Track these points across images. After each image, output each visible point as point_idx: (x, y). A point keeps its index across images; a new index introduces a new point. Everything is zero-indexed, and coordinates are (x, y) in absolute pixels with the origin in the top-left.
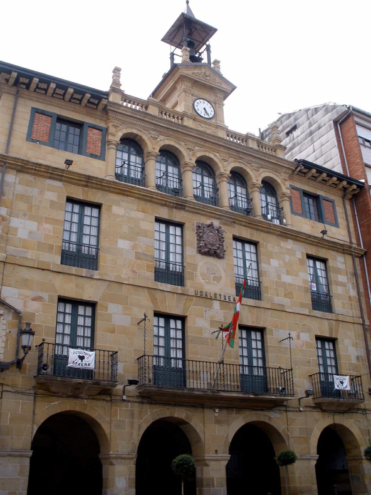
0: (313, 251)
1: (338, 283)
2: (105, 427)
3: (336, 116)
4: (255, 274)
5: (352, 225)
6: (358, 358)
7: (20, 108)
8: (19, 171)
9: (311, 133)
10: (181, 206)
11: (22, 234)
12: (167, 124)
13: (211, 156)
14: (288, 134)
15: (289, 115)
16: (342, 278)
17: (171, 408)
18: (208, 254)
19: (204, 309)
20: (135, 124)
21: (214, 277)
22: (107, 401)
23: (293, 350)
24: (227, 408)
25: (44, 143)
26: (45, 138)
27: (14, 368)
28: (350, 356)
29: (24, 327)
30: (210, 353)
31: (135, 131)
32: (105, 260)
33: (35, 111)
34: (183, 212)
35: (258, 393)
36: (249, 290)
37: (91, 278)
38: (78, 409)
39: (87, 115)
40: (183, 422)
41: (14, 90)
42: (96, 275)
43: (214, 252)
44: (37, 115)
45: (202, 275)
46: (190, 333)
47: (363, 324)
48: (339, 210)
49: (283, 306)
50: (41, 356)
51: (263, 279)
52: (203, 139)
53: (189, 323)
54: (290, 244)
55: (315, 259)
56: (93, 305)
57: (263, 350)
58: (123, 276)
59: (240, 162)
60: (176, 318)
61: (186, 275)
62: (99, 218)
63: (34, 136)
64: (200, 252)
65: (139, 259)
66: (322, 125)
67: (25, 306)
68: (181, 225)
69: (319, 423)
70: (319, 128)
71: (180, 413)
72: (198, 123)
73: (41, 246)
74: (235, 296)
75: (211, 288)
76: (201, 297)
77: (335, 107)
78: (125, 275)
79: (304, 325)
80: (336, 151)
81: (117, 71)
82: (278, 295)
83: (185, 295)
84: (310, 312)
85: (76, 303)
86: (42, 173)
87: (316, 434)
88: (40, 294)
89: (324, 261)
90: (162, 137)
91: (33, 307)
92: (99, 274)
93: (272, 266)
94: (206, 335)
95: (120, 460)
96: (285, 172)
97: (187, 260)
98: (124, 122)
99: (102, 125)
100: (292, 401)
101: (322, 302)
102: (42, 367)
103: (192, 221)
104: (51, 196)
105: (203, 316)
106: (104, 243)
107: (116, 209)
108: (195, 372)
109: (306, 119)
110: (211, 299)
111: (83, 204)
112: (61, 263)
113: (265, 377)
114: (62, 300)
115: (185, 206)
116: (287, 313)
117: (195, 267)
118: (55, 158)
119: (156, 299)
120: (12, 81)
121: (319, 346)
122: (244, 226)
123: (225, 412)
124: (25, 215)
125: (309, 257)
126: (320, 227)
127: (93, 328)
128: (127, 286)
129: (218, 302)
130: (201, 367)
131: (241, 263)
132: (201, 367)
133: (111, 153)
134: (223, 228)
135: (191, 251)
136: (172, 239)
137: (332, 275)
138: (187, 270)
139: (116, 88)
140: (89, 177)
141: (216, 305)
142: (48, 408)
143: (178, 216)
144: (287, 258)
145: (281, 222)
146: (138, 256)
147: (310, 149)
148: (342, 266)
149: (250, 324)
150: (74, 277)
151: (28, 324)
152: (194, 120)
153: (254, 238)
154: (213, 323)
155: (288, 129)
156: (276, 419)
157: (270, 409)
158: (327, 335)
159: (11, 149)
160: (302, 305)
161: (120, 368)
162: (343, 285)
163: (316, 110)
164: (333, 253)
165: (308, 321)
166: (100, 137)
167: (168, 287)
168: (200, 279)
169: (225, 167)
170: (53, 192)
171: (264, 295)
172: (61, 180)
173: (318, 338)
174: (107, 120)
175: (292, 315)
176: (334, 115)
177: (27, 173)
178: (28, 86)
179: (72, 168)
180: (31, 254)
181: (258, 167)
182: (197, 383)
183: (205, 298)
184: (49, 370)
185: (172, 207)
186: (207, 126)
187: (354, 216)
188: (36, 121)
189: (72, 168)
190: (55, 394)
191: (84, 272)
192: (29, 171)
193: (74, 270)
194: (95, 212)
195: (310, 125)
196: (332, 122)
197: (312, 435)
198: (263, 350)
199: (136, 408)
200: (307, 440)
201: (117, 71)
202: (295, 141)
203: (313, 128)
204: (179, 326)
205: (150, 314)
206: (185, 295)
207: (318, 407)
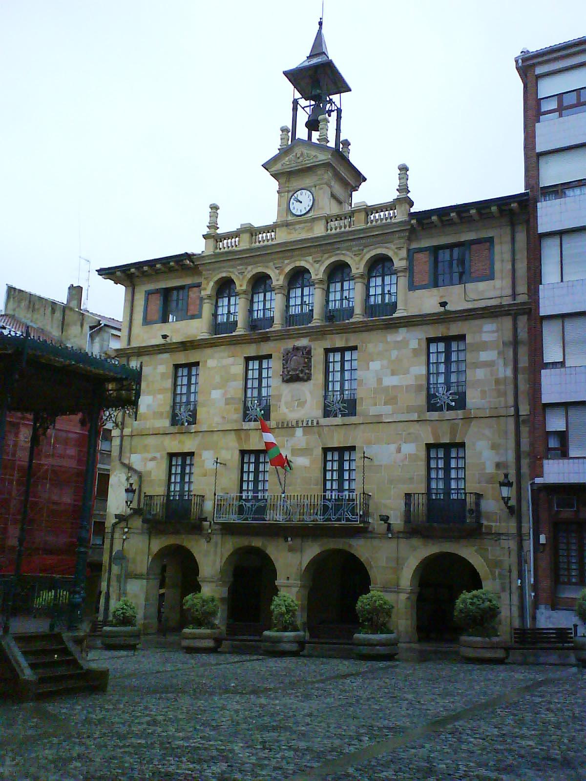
0: (439, 331)
10: (266, 338)
12: (301, 244)
28: (484, 464)
38: (341, 547)
43: (296, 375)
45: (286, 403)
47: (517, 415)
54: (402, 334)
59: (337, 254)
69: (414, 555)
71: (257, 542)
75: (292, 416)
76: (283, 427)
79: (409, 434)
90: (250, 268)
91: (151, 465)
108: (312, 505)
110: (293, 427)
115: (269, 337)
117: (279, 397)
122: (338, 333)
123: (298, 541)
129: (301, 429)
141: (299, 432)
142: (157, 545)
143: (265, 348)
144: (394, 354)
148: (486, 337)
156: (361, 548)
160: (410, 410)
165: (415, 428)
168: (284, 409)
174: (199, 274)
175: (394, 425)
177: (145, 355)
179: (448, 307)
181: (359, 250)
182: (276, 517)
185: (259, 342)
189: (448, 307)
197: (406, 565)
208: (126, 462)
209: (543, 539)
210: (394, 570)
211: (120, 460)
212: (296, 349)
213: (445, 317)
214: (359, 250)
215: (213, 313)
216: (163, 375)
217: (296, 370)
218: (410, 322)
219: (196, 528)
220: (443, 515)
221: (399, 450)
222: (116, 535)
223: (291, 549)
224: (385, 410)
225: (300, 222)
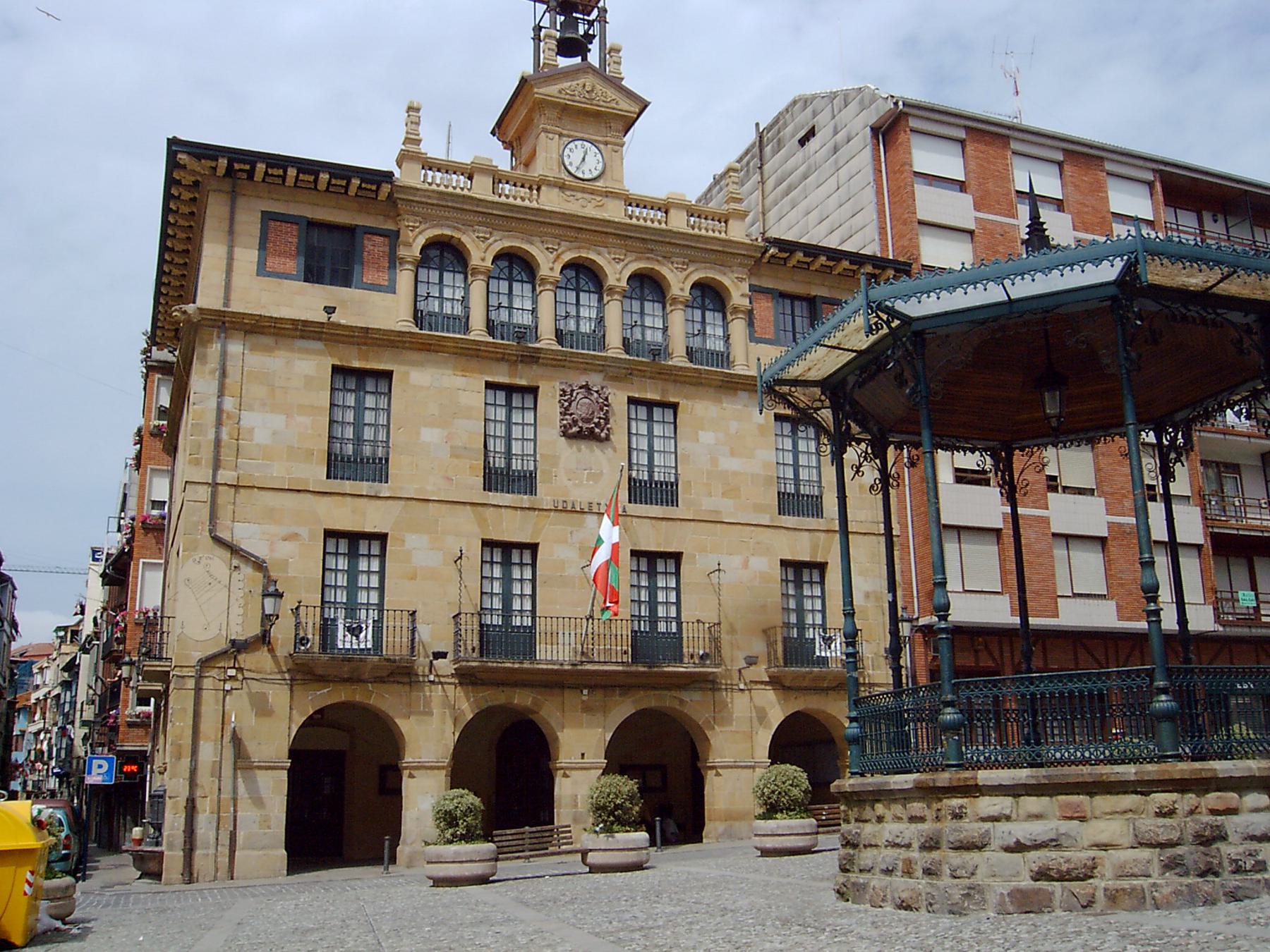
3: (873, 120)
7: (241, 217)
8: (247, 332)
9: (836, 149)
10: (532, 358)
17: (508, 690)
18: (579, 436)
19: (569, 529)
20: (447, 219)
22: (404, 683)
31: (448, 232)
33: (267, 217)
34: (535, 367)
38: (358, 698)
39: (360, 211)
41: (227, 186)
43: (587, 432)
44: (272, 224)
49: (718, 512)
52: (571, 227)
56: (382, 538)
58: (429, 488)
59: (648, 258)
64: (565, 434)
65: (457, 457)
66: (853, 134)
67: (272, 550)
71: (522, 699)
72: (568, 193)
74: (627, 503)
76: (564, 510)
80: (869, 194)
82: (710, 495)
83: (535, 509)
84: (772, 520)
86: (287, 332)
88: (295, 529)
91: (286, 550)
92: (389, 488)
95: (422, 772)
96: (740, 265)
98: (425, 219)
99: (390, 226)
105: (566, 542)
109: (830, 115)
110: (582, 512)
112: (328, 477)
116: (987, 596)
119: (485, 520)
120: (221, 171)
121: (791, 577)
123: (599, 695)
124: (264, 405)
128: (436, 505)
130: (561, 627)
132: (561, 627)
146: (455, 454)
149: (653, 548)
150: (349, 499)
152: (562, 187)
155: (802, 133)
158: (806, 558)
159: (233, 296)
160: (758, 508)
161: (424, 632)
166: (387, 249)
169: (617, 272)
172: (320, 339)
173: (784, 563)
174: (397, 216)
176: (872, 116)
178: (251, 174)
179: (335, 318)
186: (586, 196)
188: (271, 236)
189: (335, 318)
191: (364, 487)
192: (266, 330)
193: (348, 486)
196: (868, 129)
202: (812, 160)
203: (841, 136)
206: (535, 509)
208: (224, 535)
211: (211, 531)
214: (684, 263)
216: (309, 381)
217: (588, 421)
220: (500, 647)
221: (746, 565)
222: (207, 683)
224: (728, 508)
225: (583, 190)
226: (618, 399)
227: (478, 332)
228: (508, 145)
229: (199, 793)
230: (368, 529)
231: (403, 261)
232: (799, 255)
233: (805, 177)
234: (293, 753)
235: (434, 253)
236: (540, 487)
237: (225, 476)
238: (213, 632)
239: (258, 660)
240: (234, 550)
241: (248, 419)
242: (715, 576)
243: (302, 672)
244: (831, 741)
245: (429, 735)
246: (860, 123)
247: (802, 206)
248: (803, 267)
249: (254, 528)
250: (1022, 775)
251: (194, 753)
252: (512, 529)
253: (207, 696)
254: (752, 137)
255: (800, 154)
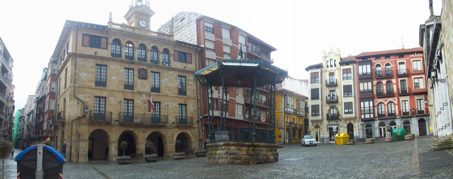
0: (180, 74)
1: (189, 85)
2: (109, 133)
3: (197, 18)
4: (158, 84)
5: (197, 63)
6: (194, 111)
9: (189, 23)
10: (133, 63)
11: (83, 78)
13: (145, 43)
14: (181, 21)
15: (182, 13)
16: (191, 83)
21: (143, 86)
23: (171, 109)
24: (146, 128)
25: (88, 46)
26: (88, 44)
27: (83, 118)
29: (85, 107)
30: (141, 110)
31: (117, 37)
32: (108, 83)
35: (157, 122)
36: (156, 90)
37: (104, 90)
40: (131, 132)
42: (106, 88)
46: (135, 105)
47: (198, 99)
48: (193, 58)
50: (90, 114)
51: (161, 85)
53: (135, 102)
54: (172, 72)
55: (181, 77)
56: (105, 98)
57: (160, 109)
60: (131, 100)
61: (134, 86)
62: (106, 70)
63: (84, 44)
68: (133, 69)
69: (177, 132)
70: (192, 21)
71: (131, 129)
73: (89, 81)
75: (142, 90)
77: (197, 14)
78: (115, 88)
81: (111, 13)
85: (100, 97)
87: (176, 135)
88: (89, 96)
89: (185, 77)
90: (127, 38)
91: (88, 100)
93: (164, 81)
94: (140, 105)
97: (135, 81)
99: (106, 36)
100: (168, 125)
101: (182, 92)
102: (91, 117)
103: (136, 68)
104: (91, 64)
106: (108, 78)
107: (112, 67)
111: (101, 65)
113: (159, 118)
114: (96, 97)
117: (137, 83)
118: (91, 51)
123: (145, 129)
125: (179, 76)
126: (184, 65)
127: (105, 104)
131: (153, 80)
133: (109, 47)
134: (148, 69)
135: (136, 78)
136: (130, 74)
137: (187, 82)
138: (135, 84)
139: (110, 22)
140: (103, 57)
141: (144, 95)
142: (92, 129)
143: (132, 66)
144: (170, 77)
145: (169, 65)
146: (119, 81)
147: (188, 29)
151: (87, 106)
152: (139, 29)
153: (159, 72)
154: (142, 101)
156: (163, 131)
157: (160, 128)
158: (183, 103)
159: (77, 50)
160: (175, 94)
161: (113, 116)
162: (191, 85)
163: (191, 14)
164: (189, 74)
165: (176, 99)
167: (129, 91)
168: (139, 87)
170: (91, 63)
171: (161, 91)
173: (179, 104)
176: (196, 18)
180: (86, 84)
183: (140, 93)
184: (93, 118)
187: (199, 59)
190: (95, 125)
191: (102, 88)
193: (99, 87)
194: (105, 68)
195: (189, 19)
198: (160, 109)
199: (118, 128)
200: (173, 137)
201: (111, 13)
204: (132, 102)
205: (123, 100)
207: (177, 127)
208: (77, 96)
209: (203, 129)
210: (171, 137)
212: (143, 69)
213: (183, 71)
215: (375, 58)
218: (175, 70)
219: (109, 123)
220: (183, 122)
221: (172, 104)
222: (74, 125)
223: (143, 132)
224: (169, 93)
226: (149, 71)
227: (123, 58)
228: (127, 20)
229: (72, 145)
230: (103, 96)
231: (109, 43)
232: (183, 44)
233: (182, 27)
234: (89, 139)
235: (114, 42)
236: (135, 89)
237: (77, 85)
238: (74, 115)
239: (84, 121)
240: (78, 99)
241: (81, 74)
242: (167, 107)
243: (91, 123)
244: (3, 158)
245: (114, 135)
246: (194, 19)
247: (181, 33)
248: (184, 46)
249: (82, 95)
250: (235, 143)
251: (71, 138)
252: (129, 97)
253: (74, 127)
254: (171, 18)
255: (181, 23)
